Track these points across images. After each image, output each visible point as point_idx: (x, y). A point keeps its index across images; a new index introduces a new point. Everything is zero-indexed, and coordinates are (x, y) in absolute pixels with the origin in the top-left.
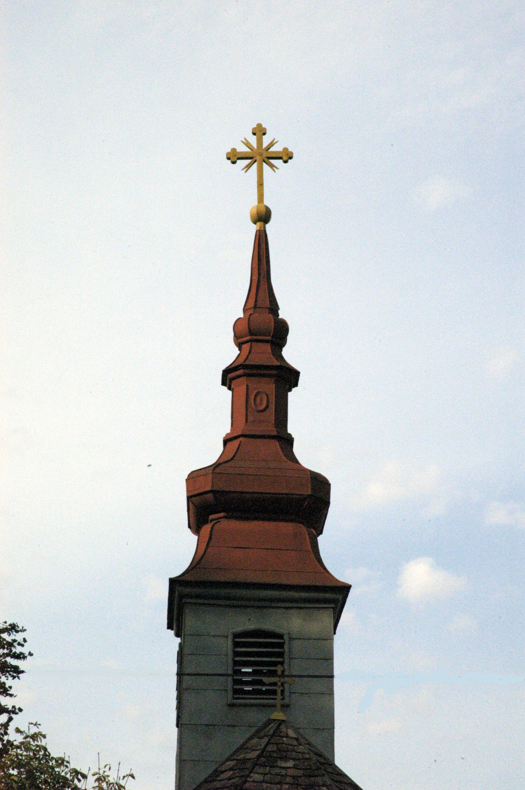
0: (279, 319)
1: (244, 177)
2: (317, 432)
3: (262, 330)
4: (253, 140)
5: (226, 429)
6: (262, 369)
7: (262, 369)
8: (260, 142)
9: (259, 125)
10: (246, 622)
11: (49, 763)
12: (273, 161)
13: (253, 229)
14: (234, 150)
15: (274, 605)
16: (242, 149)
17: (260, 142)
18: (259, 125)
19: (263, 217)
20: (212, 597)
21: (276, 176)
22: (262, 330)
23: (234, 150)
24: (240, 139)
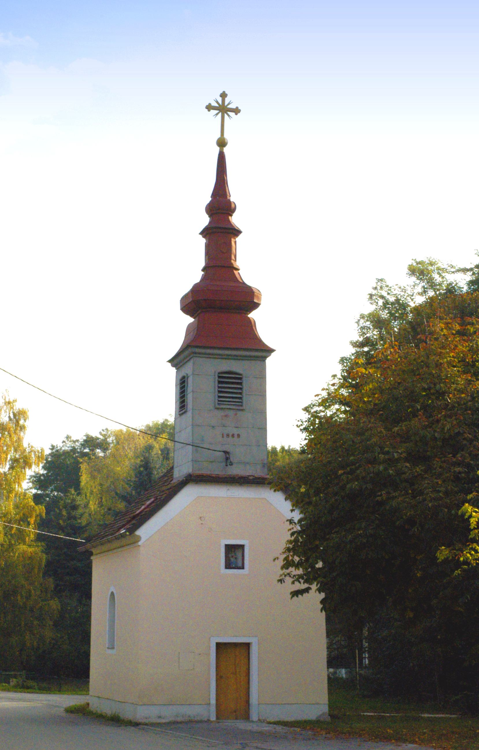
0: (229, 222)
1: (213, 119)
2: (250, 264)
3: (220, 207)
4: (220, 100)
5: (203, 264)
6: (220, 229)
7: (220, 229)
8: (223, 101)
9: (224, 92)
10: (226, 366)
11: (378, 349)
12: (229, 113)
13: (217, 149)
14: (210, 104)
15: (201, 356)
16: (215, 104)
17: (223, 101)
18: (224, 92)
19: (222, 143)
20: (210, 354)
21: (231, 120)
22: (220, 207)
23: (210, 104)
24: (214, 99)
